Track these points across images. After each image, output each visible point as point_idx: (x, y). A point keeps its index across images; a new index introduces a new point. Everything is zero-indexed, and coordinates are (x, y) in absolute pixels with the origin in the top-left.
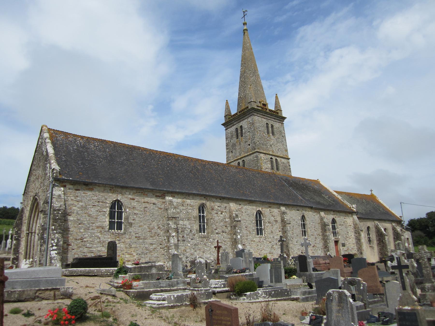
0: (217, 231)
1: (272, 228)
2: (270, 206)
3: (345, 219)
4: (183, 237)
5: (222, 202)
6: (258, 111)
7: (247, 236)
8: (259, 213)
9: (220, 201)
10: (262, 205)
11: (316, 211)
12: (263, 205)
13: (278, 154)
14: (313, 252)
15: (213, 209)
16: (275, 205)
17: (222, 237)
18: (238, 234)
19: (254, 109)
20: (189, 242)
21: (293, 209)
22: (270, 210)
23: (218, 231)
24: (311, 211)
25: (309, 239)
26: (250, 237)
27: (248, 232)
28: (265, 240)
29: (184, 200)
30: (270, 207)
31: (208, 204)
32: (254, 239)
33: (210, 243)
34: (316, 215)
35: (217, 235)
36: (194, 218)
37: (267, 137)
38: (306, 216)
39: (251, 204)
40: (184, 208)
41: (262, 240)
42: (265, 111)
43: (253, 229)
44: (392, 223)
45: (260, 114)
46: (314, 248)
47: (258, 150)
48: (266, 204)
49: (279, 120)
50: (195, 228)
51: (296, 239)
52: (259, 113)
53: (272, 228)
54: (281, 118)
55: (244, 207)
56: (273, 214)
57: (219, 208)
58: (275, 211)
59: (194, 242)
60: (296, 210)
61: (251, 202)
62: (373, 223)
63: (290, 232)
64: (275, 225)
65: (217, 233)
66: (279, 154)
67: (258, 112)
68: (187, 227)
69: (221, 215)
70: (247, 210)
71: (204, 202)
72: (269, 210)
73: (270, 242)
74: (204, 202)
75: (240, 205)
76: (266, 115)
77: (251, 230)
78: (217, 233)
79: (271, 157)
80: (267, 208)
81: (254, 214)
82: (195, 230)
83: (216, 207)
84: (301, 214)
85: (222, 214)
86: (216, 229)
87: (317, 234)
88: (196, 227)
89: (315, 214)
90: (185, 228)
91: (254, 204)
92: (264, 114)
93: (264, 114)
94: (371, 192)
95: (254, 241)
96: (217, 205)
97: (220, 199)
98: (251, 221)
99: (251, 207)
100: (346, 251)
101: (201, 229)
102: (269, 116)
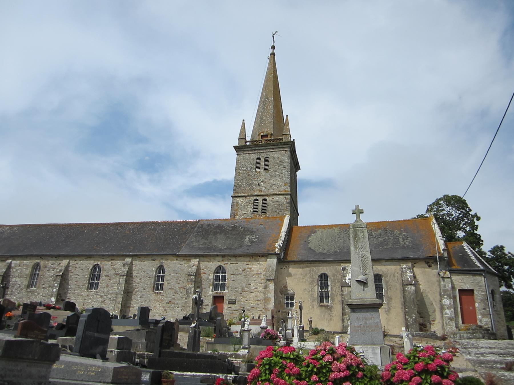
0: (44, 286)
1: (109, 282)
2: (113, 258)
3: (247, 266)
4: (12, 291)
5: (57, 260)
6: (244, 147)
7: (75, 290)
8: (161, 269)
9: (55, 259)
10: (103, 258)
11: (186, 258)
12: (104, 258)
13: (271, 192)
14: (165, 310)
15: (46, 267)
16: (119, 257)
17: (48, 291)
18: (54, 288)
19: (237, 148)
20: (15, 295)
21: (146, 259)
22: (112, 263)
23: (45, 286)
24: (177, 259)
25: (163, 293)
26: (79, 291)
27: (77, 287)
28: (95, 294)
29: (22, 261)
30: (112, 260)
31: (42, 263)
32: (82, 294)
33: (34, 296)
34: (185, 263)
35: (43, 290)
36: (26, 275)
37: (254, 175)
38: (165, 267)
39: (89, 259)
40: (20, 268)
41: (91, 294)
42: (272, 144)
43: (84, 283)
44: (401, 264)
45: (248, 150)
46: (169, 305)
47: (236, 194)
48: (108, 257)
49: (282, 148)
50: (24, 284)
51: (141, 294)
52: (245, 150)
53: (109, 282)
54: (284, 145)
55: (56, 262)
56: (114, 266)
57: (52, 265)
58: (119, 264)
59: (20, 295)
60: (151, 260)
61: (88, 257)
62: (398, 267)
63: (121, 285)
64: (114, 278)
65: (44, 288)
66: (272, 192)
67: (245, 148)
68: (18, 283)
69: (53, 272)
70: (82, 265)
71: (39, 261)
72: (110, 263)
73: (101, 297)
74: (39, 261)
75: (76, 260)
76: (257, 148)
77: (81, 284)
78: (44, 288)
79: (255, 198)
80: (109, 261)
81: (89, 268)
82: (24, 286)
83: (50, 264)
84: (157, 264)
85: (53, 270)
86: (44, 285)
87: (179, 287)
88: (26, 283)
89: (183, 263)
90: (15, 284)
91: (92, 258)
92: (253, 149)
93: (253, 149)
94: (358, 217)
95: (82, 295)
96: (241, 265)
97: (56, 257)
98: (83, 275)
99: (87, 262)
100: (237, 310)
101: (323, 296)
102: (263, 148)
